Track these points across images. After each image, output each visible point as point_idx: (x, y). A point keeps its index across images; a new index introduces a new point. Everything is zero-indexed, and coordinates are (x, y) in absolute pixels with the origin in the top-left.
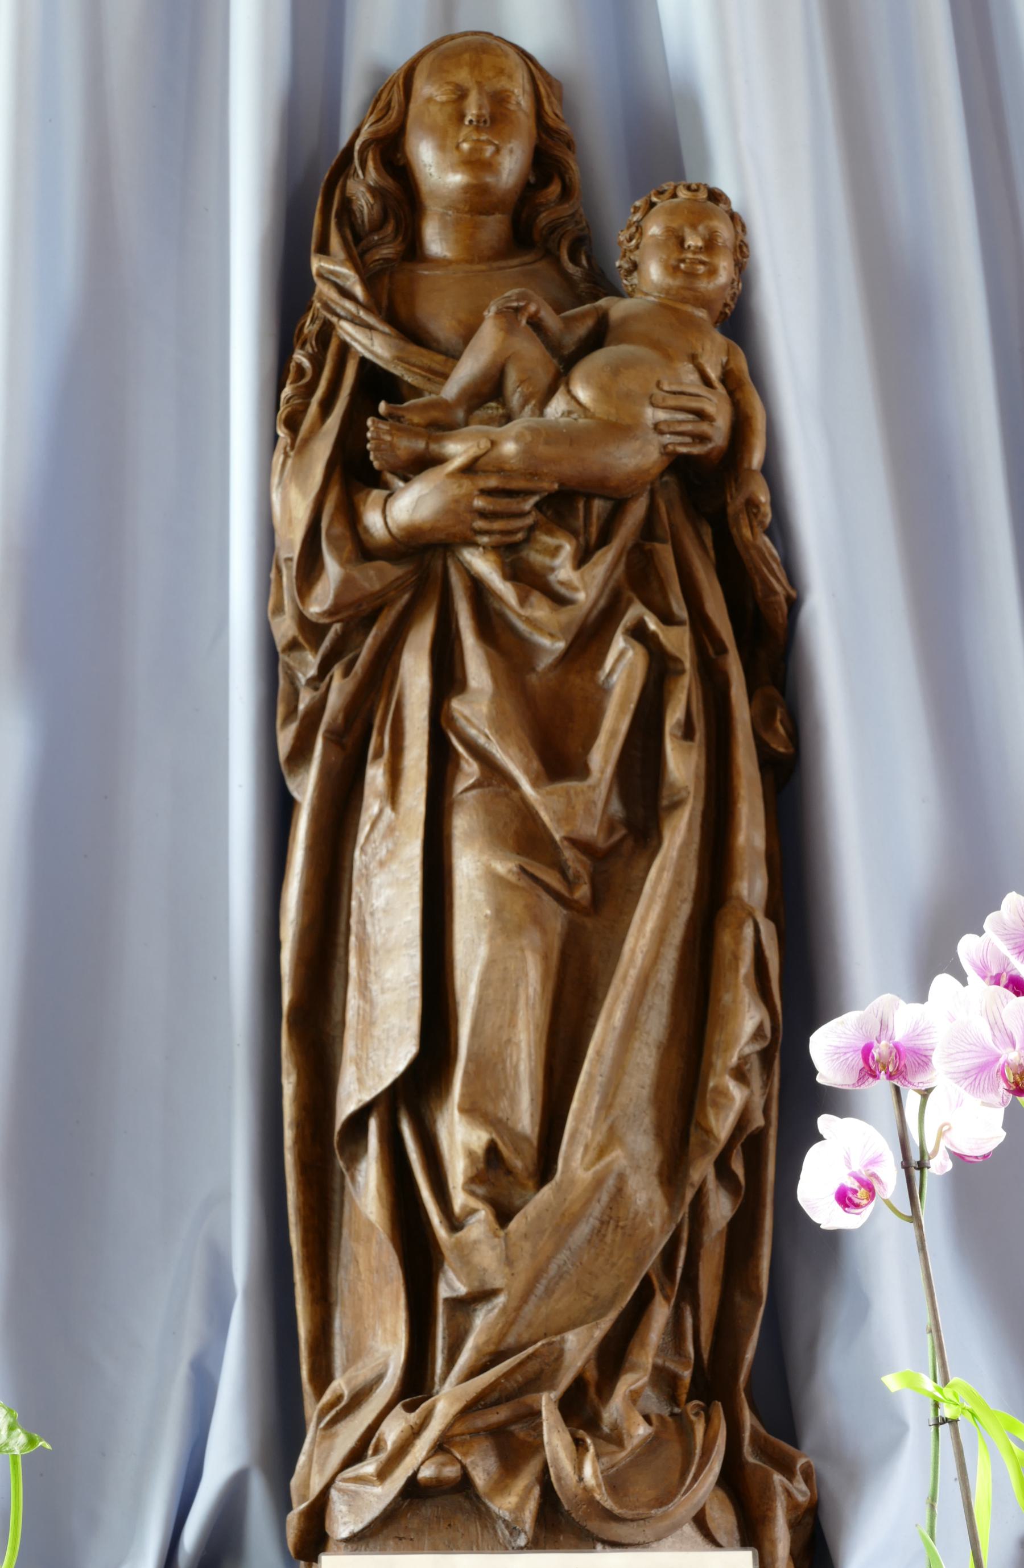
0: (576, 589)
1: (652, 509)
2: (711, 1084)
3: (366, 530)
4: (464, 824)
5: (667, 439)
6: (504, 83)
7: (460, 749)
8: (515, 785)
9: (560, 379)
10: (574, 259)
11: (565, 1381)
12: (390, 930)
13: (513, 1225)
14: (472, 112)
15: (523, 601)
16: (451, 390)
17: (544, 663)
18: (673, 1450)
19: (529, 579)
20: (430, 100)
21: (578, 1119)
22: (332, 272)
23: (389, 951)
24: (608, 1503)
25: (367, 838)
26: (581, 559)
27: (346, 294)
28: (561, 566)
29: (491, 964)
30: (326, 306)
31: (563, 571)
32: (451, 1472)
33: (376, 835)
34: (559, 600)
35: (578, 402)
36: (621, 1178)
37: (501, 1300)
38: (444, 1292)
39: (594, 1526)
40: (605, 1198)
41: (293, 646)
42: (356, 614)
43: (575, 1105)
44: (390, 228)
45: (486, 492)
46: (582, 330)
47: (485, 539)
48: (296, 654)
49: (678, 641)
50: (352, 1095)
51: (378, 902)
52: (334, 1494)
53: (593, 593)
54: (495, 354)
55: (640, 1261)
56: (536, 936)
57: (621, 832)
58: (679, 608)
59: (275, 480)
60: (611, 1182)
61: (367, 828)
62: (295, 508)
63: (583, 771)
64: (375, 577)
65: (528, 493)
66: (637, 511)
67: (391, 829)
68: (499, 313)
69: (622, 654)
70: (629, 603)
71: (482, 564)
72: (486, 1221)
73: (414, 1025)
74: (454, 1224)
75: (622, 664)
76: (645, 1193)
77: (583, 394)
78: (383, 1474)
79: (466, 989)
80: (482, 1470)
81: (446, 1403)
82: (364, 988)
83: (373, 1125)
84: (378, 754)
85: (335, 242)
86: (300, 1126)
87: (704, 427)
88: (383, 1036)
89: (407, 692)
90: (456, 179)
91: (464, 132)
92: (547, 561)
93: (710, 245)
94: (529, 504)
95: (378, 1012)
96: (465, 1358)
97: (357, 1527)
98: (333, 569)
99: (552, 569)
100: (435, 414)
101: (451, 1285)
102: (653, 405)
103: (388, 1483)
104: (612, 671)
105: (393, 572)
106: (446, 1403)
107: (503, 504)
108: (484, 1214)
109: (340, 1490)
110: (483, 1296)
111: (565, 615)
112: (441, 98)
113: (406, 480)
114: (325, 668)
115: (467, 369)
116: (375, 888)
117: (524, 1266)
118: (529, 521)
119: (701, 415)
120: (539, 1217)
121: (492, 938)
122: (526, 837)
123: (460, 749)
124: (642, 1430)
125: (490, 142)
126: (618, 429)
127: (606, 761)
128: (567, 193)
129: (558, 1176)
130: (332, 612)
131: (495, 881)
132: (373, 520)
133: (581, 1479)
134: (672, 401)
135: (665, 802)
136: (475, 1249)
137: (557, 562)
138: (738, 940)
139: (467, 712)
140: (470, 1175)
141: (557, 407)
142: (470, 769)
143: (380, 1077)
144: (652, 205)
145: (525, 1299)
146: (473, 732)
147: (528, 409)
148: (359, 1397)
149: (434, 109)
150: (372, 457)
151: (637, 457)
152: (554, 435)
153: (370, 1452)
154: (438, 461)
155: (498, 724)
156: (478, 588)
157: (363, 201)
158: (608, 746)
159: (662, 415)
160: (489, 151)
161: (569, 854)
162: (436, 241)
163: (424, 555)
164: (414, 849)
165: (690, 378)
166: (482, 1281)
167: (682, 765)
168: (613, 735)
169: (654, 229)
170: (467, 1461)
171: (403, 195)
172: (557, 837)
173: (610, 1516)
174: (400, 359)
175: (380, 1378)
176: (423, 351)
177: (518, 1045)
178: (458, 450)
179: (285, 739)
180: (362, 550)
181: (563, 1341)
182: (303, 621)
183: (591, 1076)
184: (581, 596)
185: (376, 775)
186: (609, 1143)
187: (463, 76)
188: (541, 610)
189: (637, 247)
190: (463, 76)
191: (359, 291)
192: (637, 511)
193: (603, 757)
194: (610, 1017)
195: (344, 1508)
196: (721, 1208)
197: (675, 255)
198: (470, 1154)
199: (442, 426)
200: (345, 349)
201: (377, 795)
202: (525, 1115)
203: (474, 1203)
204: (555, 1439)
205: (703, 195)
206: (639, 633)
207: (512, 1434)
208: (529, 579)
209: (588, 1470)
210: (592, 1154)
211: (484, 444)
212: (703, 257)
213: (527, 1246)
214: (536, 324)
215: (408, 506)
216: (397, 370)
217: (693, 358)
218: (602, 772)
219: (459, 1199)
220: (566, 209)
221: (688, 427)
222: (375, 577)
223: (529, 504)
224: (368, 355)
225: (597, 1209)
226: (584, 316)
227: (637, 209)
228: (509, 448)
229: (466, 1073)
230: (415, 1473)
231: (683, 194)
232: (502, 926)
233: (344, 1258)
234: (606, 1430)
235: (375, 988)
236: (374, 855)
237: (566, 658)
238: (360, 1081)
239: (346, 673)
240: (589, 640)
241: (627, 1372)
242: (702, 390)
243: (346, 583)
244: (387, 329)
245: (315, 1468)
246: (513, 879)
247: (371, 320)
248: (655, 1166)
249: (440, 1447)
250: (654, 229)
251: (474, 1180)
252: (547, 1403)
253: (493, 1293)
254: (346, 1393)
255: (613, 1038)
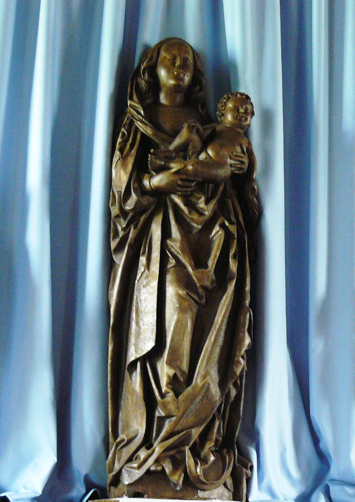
0: (205, 211)
1: (225, 188)
2: (236, 359)
3: (144, 186)
4: (169, 278)
5: (233, 169)
6: (187, 55)
7: (170, 255)
8: (185, 267)
9: (204, 148)
10: (203, 110)
11: (191, 443)
12: (146, 307)
13: (180, 398)
14: (178, 63)
15: (190, 213)
16: (172, 147)
17: (195, 231)
18: (220, 464)
19: (192, 206)
20: (165, 57)
21: (200, 368)
22: (135, 106)
23: (146, 313)
24: (204, 480)
25: (140, 278)
26: (207, 202)
27: (139, 113)
28: (201, 203)
29: (178, 321)
30: (132, 116)
31: (202, 205)
32: (159, 468)
33: (143, 278)
34: (201, 213)
35: (209, 155)
36: (209, 385)
37: (174, 419)
38: (157, 414)
39: (198, 485)
40: (204, 390)
41: (117, 216)
42: (138, 210)
43: (199, 364)
44: (150, 94)
45: (181, 180)
46: (208, 132)
47: (180, 193)
48: (118, 219)
49: (233, 229)
50: (132, 355)
51: (143, 298)
52: (123, 470)
53: (210, 212)
54: (187, 139)
55: (213, 409)
56: (190, 313)
57: (215, 285)
58: (233, 219)
59: (114, 166)
60: (206, 385)
61: (140, 275)
62: (121, 177)
63: (206, 266)
64: (146, 200)
65: (193, 181)
66: (221, 188)
67: (147, 277)
68: (188, 127)
69: (218, 232)
70: (219, 217)
71: (178, 200)
72: (172, 395)
73: (154, 337)
74: (163, 396)
75: (217, 234)
76: (215, 390)
77: (210, 152)
78: (139, 467)
79: (170, 327)
80: (168, 468)
81: (158, 449)
82: (137, 323)
83: (139, 364)
84: (144, 253)
85: (135, 97)
86: (113, 358)
87: (243, 166)
88: (143, 339)
89: (153, 235)
90: (172, 82)
91: (175, 69)
92: (196, 200)
93: (246, 110)
94: (193, 185)
95: (142, 331)
96: (162, 434)
97: (131, 482)
98: (134, 197)
99: (198, 204)
100: (167, 154)
101: (160, 412)
102: (231, 159)
103: (141, 470)
104: (214, 236)
105: (151, 199)
106: (158, 449)
107: (187, 184)
108: (171, 394)
109: (125, 470)
110: (169, 416)
111: (202, 219)
112: (168, 57)
113: (157, 173)
114: (128, 225)
115: (177, 142)
116: (141, 293)
117: (181, 410)
118: (192, 189)
119: (242, 163)
120: (187, 396)
121: (178, 314)
122: (185, 282)
123: (170, 255)
124: (212, 458)
125: (182, 73)
126: (221, 164)
127: (213, 263)
128: (201, 89)
129: (193, 384)
130: (132, 210)
131: (179, 297)
132: (146, 183)
133: (196, 472)
134: (235, 158)
135: (228, 277)
136: (168, 402)
137: (199, 201)
138: (245, 318)
139: (172, 245)
140: (168, 381)
141: (202, 156)
142: (172, 262)
143: (142, 351)
144: (229, 98)
145: (181, 418)
146: (173, 250)
147: (194, 156)
148: (130, 441)
149: (166, 61)
150: (149, 165)
151: (224, 172)
152: (202, 163)
153: (134, 459)
154: (169, 168)
155: (182, 249)
156: (176, 207)
157: (143, 84)
158: (214, 259)
159: (233, 162)
160: (182, 75)
161: (200, 291)
162: (163, 99)
163: (160, 195)
164: (155, 284)
165: (238, 149)
166: (169, 413)
167: (233, 266)
168: (215, 256)
169: (230, 105)
170: (164, 465)
171: (155, 84)
172: (198, 285)
173: (204, 483)
174: (157, 136)
175: (136, 436)
176: (161, 133)
177: (184, 346)
178: (175, 167)
179: (114, 244)
180: (142, 191)
181: (191, 432)
182: (122, 209)
183: (204, 356)
184: (206, 213)
185: (143, 260)
186: (207, 373)
187: (175, 52)
188: (195, 216)
189: (224, 109)
190: (175, 52)
191: (142, 112)
192: (221, 188)
193: (212, 263)
194: (210, 340)
195: (127, 475)
196: (233, 393)
197: (237, 114)
198: (169, 376)
199: (169, 159)
200: (137, 129)
201: (143, 266)
202: (185, 366)
203: (169, 390)
204: (190, 461)
205: (244, 97)
206: (223, 226)
207: (175, 457)
208: (192, 206)
209: (198, 470)
210: (202, 378)
211: (183, 166)
212: (244, 116)
213: (183, 404)
214: (198, 131)
215: (157, 180)
216: (153, 138)
217: (241, 145)
218: (212, 267)
219: (164, 389)
220: (201, 94)
221: (239, 166)
222: (146, 200)
223: (193, 185)
224: (144, 132)
225: (202, 394)
226: (209, 128)
227: (225, 98)
228: (190, 167)
229: (169, 352)
230: (149, 468)
231: (239, 96)
232: (182, 310)
233: (123, 398)
234: (202, 457)
235: (141, 323)
236: (142, 283)
237: (201, 230)
238: (136, 351)
239: (135, 228)
240: (208, 225)
241: (208, 441)
242: (243, 155)
243: (138, 203)
244: (151, 126)
245: (116, 461)
246: (185, 297)
247: (147, 122)
248: (217, 381)
249: (157, 461)
250: (230, 105)
251: (168, 384)
252: (187, 449)
253: (173, 416)
254: (126, 439)
255: (210, 345)
